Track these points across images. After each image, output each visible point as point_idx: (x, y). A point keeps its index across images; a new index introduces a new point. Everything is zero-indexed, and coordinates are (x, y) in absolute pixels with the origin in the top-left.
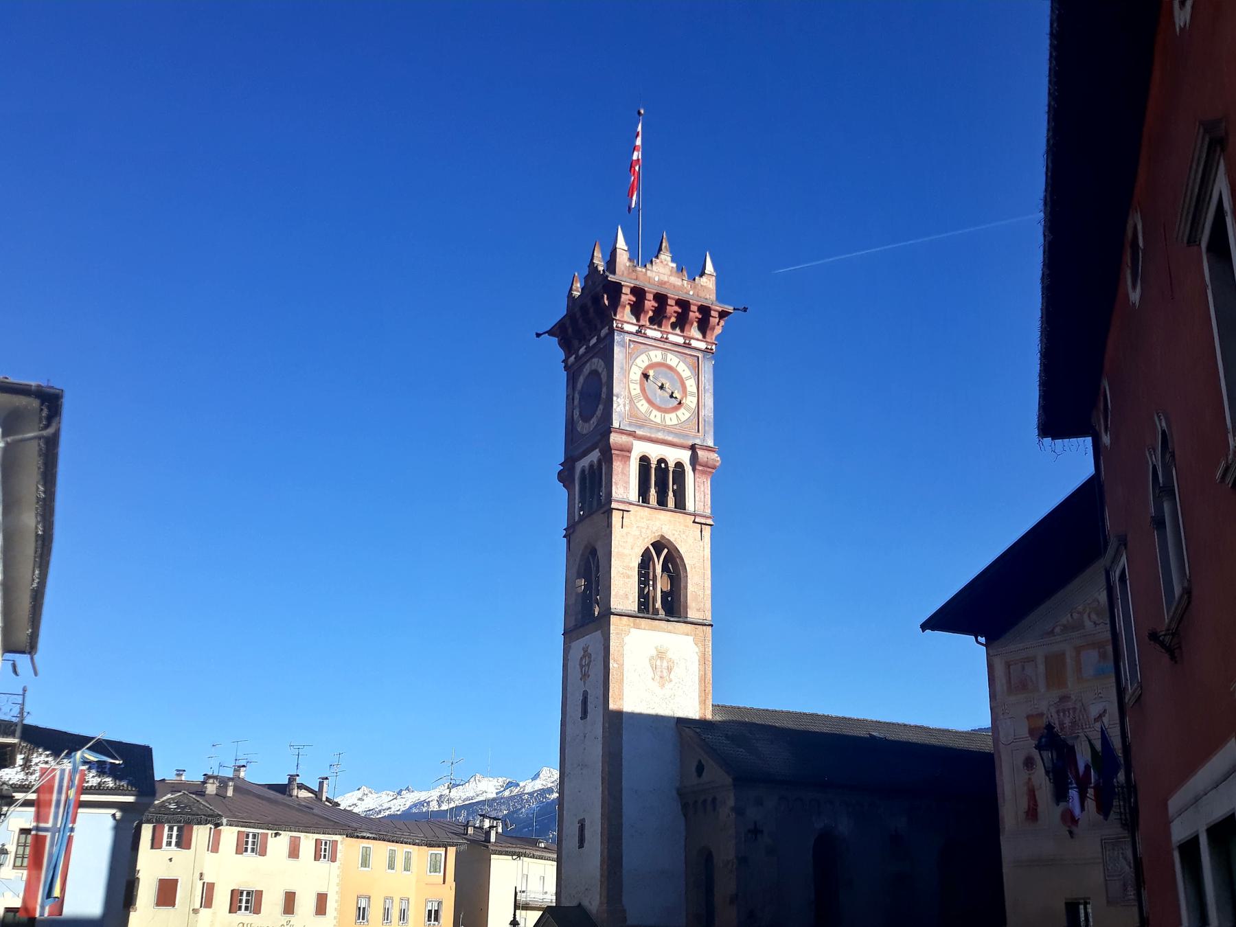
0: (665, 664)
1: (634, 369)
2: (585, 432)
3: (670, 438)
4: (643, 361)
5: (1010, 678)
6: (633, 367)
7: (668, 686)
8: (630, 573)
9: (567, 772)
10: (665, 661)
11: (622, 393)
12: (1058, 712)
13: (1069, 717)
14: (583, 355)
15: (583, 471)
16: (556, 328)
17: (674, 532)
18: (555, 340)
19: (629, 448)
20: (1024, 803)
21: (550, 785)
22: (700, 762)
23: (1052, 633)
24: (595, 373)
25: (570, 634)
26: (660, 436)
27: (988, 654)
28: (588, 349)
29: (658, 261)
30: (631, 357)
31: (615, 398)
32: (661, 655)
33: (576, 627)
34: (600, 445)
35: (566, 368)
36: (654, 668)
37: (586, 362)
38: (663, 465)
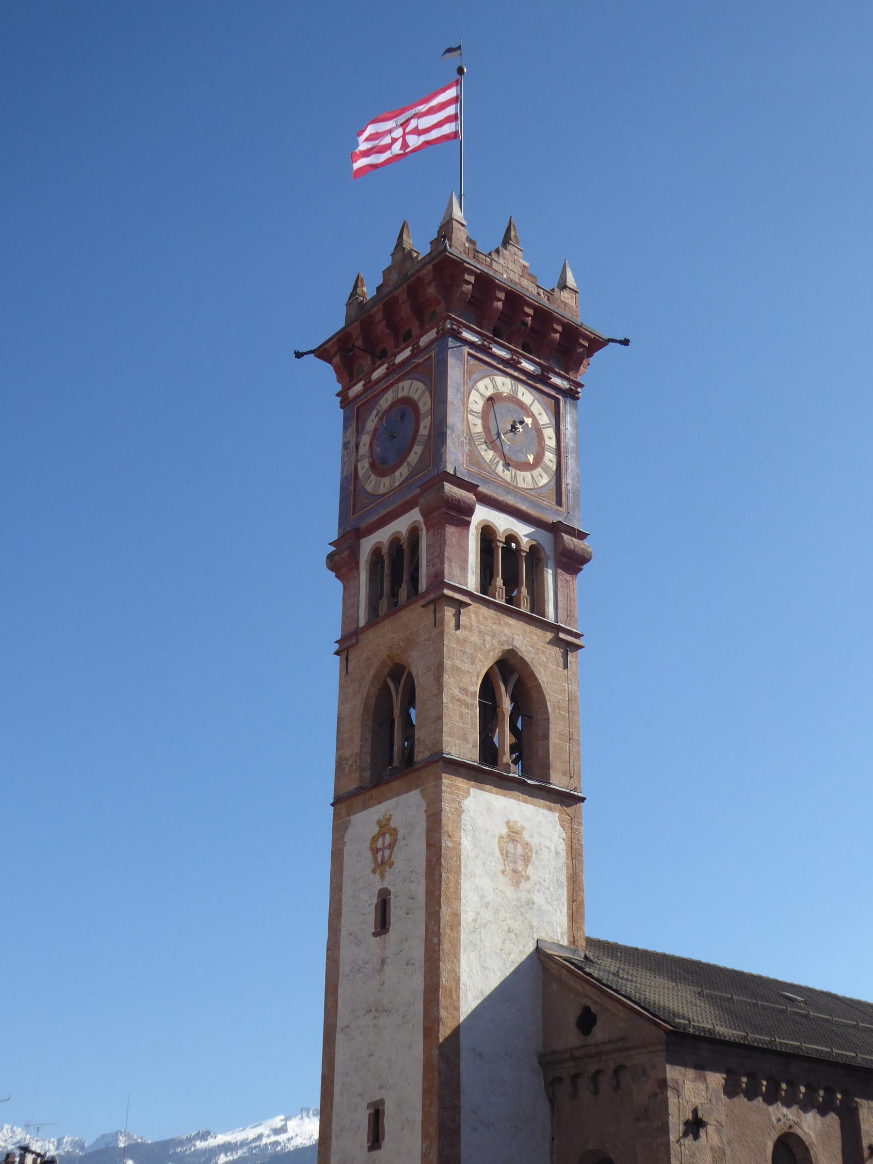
0: (520, 851)
1: (474, 396)
2: (382, 490)
3: (524, 507)
6: (473, 392)
7: (524, 885)
8: (469, 700)
9: (340, 1024)
10: (519, 846)
14: (357, 397)
15: (376, 552)
22: (586, 1010)
24: (408, 404)
26: (510, 500)
29: (506, 252)
31: (449, 432)
32: (514, 834)
33: (362, 790)
34: (422, 501)
36: (505, 855)
38: (514, 545)
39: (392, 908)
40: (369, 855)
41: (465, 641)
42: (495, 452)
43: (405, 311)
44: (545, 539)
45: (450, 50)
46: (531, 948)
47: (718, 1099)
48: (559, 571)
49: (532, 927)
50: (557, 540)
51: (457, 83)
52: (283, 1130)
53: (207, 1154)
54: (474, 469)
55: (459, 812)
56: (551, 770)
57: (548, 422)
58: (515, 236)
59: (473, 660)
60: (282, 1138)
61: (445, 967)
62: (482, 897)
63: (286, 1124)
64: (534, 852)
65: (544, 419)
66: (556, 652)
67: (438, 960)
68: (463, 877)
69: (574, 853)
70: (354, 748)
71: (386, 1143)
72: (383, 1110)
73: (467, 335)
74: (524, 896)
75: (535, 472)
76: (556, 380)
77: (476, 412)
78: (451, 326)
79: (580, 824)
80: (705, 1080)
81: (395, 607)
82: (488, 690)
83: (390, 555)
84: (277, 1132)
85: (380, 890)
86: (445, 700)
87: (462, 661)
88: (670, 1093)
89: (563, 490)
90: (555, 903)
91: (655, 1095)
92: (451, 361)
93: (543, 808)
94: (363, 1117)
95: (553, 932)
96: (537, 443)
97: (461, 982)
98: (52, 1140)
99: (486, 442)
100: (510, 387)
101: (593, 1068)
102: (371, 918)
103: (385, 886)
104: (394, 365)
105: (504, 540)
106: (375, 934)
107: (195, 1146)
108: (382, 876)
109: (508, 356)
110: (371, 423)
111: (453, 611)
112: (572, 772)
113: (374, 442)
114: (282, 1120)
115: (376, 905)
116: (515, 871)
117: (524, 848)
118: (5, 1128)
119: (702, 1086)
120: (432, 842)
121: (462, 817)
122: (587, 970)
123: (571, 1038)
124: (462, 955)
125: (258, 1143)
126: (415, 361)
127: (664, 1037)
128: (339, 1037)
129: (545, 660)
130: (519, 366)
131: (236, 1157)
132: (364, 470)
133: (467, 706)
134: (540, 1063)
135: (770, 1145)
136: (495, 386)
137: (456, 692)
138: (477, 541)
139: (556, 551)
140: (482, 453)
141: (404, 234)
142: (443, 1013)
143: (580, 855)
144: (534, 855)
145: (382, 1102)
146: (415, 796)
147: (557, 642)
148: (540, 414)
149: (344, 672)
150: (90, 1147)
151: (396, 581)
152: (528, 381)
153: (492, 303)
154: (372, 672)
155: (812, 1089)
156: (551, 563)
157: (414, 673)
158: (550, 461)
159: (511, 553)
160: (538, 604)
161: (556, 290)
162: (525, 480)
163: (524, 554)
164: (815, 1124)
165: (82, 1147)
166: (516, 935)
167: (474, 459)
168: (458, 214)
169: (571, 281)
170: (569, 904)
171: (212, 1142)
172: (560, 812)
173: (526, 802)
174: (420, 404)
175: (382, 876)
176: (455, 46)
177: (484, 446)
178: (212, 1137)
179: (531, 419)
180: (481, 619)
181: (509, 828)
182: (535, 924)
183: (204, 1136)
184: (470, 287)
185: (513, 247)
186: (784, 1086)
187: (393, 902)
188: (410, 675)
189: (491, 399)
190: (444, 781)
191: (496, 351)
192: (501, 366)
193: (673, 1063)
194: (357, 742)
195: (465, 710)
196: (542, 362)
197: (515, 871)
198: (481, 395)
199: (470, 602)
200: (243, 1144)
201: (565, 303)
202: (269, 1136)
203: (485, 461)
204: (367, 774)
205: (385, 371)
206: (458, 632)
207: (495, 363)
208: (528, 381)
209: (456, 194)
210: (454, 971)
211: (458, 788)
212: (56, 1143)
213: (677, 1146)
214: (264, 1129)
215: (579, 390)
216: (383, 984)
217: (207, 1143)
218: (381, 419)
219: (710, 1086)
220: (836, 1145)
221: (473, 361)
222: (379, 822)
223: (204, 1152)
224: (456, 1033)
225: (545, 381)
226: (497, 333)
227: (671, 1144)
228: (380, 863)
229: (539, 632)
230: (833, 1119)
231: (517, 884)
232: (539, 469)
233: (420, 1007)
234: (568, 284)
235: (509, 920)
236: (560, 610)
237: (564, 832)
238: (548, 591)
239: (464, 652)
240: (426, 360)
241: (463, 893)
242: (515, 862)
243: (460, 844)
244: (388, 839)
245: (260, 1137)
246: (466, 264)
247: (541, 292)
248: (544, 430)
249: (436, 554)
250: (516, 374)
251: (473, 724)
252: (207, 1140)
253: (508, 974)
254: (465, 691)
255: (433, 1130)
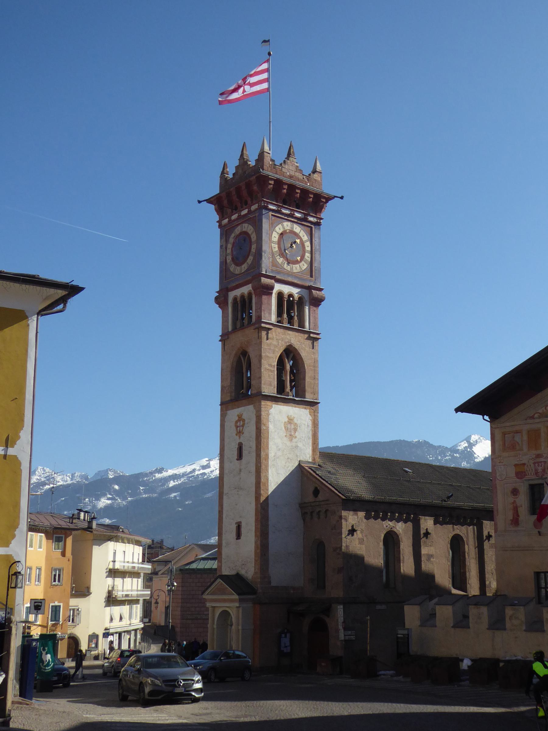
0: (293, 427)
2: (237, 272)
3: (296, 281)
4: (280, 229)
5: (505, 441)
7: (294, 440)
8: (272, 369)
11: (268, 250)
12: (534, 463)
13: (541, 466)
14: (234, 220)
15: (235, 299)
16: (213, 199)
17: (298, 343)
18: (212, 207)
19: (272, 286)
20: (510, 516)
21: (43, 479)
22: (316, 488)
23: (532, 417)
24: (245, 235)
25: (226, 405)
26: (290, 279)
27: (491, 427)
28: (240, 217)
29: (289, 161)
30: (272, 227)
31: (263, 254)
32: (290, 421)
33: (231, 401)
35: (220, 226)
36: (287, 429)
37: (238, 225)
38: (291, 299)
39: (243, 450)
40: (235, 428)
41: (271, 344)
42: (283, 258)
43: (245, 193)
44: (305, 293)
45: (265, 41)
46: (297, 464)
47: (362, 521)
48: (311, 306)
49: (297, 456)
50: (311, 293)
51: (268, 61)
52: (208, 466)
53: (162, 481)
54: (274, 268)
55: (268, 415)
56: (306, 393)
57: (307, 239)
58: (293, 152)
59: (274, 352)
60: (207, 471)
61: (263, 475)
62: (277, 447)
63: (209, 463)
64: (298, 426)
65: (305, 238)
66: (309, 342)
67: (260, 472)
68: (270, 439)
69: (315, 425)
70: (228, 382)
71: (242, 537)
72: (241, 525)
73: (271, 207)
74: (294, 444)
75: (301, 264)
76: (311, 219)
77: (275, 242)
78: (264, 204)
79: (318, 413)
80: (357, 514)
81: (243, 327)
82: (281, 363)
83: (241, 301)
84: (204, 467)
85: (239, 443)
86: (262, 370)
87: (270, 353)
88: (343, 521)
89: (313, 270)
90: (307, 445)
91: (338, 521)
92: (264, 220)
93: (303, 408)
94: (234, 527)
95: (306, 457)
96: (302, 250)
97: (269, 479)
98: (68, 475)
99: (279, 255)
100: (290, 226)
101: (318, 510)
102: (236, 453)
103: (241, 441)
104: (241, 215)
105: (287, 297)
106: (237, 460)
107: (155, 476)
108: (240, 437)
109: (289, 213)
110: (231, 240)
111: (266, 332)
112: (315, 392)
113: (233, 249)
114: (207, 461)
115: (238, 448)
116: (290, 435)
117: (294, 426)
118: (39, 468)
119: (356, 517)
120: (258, 427)
121: (269, 416)
122: (317, 472)
123: (310, 498)
124: (269, 470)
125: (193, 474)
126: (249, 216)
127: (341, 501)
128: (225, 497)
129: (304, 347)
130: (294, 216)
131: (180, 482)
132: (230, 260)
133: (272, 371)
134: (299, 507)
135: (383, 536)
136: (283, 228)
137: (267, 366)
138: (275, 300)
139: (310, 298)
140: (278, 260)
141: (244, 150)
142: (262, 492)
143: (318, 425)
144: (298, 428)
145: (240, 522)
146: (251, 407)
147: (309, 338)
148: (304, 236)
149: (223, 349)
150: (91, 478)
151: (243, 311)
152: (298, 222)
153: (282, 191)
154: (234, 352)
155: (401, 514)
156: (308, 303)
157: (251, 356)
158: (308, 257)
159: (291, 304)
160: (301, 324)
161: (312, 174)
162: (296, 268)
163: (296, 302)
164: (402, 526)
165: (86, 479)
166: (291, 460)
167: (274, 264)
168: (266, 148)
169: (319, 168)
170: (312, 445)
171: (165, 474)
172: (310, 409)
173: (295, 407)
174: (252, 237)
175: (240, 437)
176: (267, 40)
177: (279, 257)
178: (165, 471)
179: (299, 240)
180: (278, 334)
181: (288, 418)
182: (298, 455)
183: (160, 471)
184: (272, 186)
185: (292, 158)
186: (389, 514)
187: (244, 448)
188: (249, 355)
189: (282, 234)
190: (262, 403)
191: (284, 211)
192: (286, 218)
193: (345, 510)
194: (229, 381)
195: (270, 373)
196: (304, 212)
197: (290, 435)
198: (277, 233)
199: (273, 328)
200: (184, 475)
201: (316, 180)
202: (199, 470)
203: (279, 263)
204: (233, 394)
205: (237, 217)
206: (268, 341)
207: (283, 217)
208: (298, 222)
209: (267, 139)
210: (267, 476)
211: (268, 405)
212: (71, 476)
213: (345, 539)
214: (196, 466)
215: (321, 221)
216: (240, 479)
217: (162, 474)
218: (236, 239)
219: (359, 517)
220: (410, 533)
221: (273, 218)
222: (238, 415)
223: (161, 480)
224: (267, 498)
225: (305, 220)
226: (285, 202)
227: (343, 539)
228: (239, 431)
229: (302, 335)
230: (410, 524)
231: (291, 440)
232: (303, 262)
233: (254, 489)
234: (317, 170)
235: (288, 454)
236: (311, 324)
237: (311, 417)
238: (306, 320)
239: (270, 349)
240: (253, 217)
241: (270, 446)
242: (291, 432)
243: (269, 427)
244: (241, 423)
245: (194, 470)
246: (270, 177)
247: (305, 177)
248: (305, 243)
249: (259, 307)
250: (293, 220)
251: (274, 378)
252: (162, 473)
253: (287, 475)
254: (270, 365)
255: (258, 534)
